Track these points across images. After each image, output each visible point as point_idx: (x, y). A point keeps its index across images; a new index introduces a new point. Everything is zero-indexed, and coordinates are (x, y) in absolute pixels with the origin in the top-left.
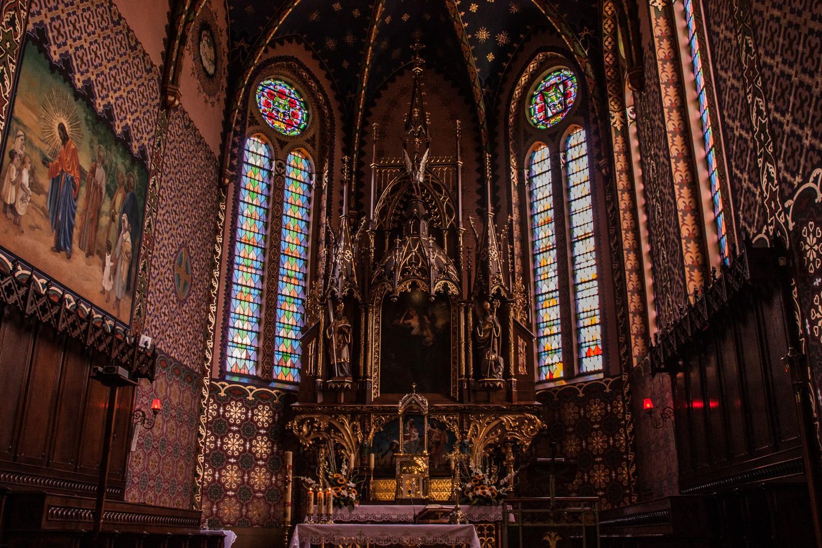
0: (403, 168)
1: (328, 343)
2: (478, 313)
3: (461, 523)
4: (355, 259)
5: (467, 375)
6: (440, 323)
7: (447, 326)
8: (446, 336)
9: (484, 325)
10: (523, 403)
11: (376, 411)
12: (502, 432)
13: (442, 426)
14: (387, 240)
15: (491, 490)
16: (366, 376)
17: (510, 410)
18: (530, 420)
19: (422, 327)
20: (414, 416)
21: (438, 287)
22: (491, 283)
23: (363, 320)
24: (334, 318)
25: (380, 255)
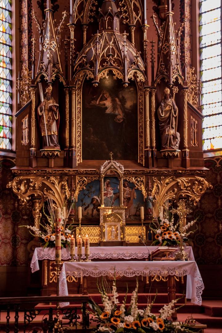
1: (39, 119)
2: (160, 98)
3: (186, 260)
4: (59, 48)
5: (151, 147)
6: (129, 104)
7: (135, 107)
8: (133, 115)
9: (165, 107)
10: (194, 168)
11: (80, 174)
12: (178, 191)
13: (132, 186)
14: (85, 33)
15: (176, 235)
16: (71, 146)
17: (184, 174)
18: (199, 182)
19: (114, 107)
20: (113, 178)
21: (129, 75)
22: (171, 73)
23: (67, 100)
24: (44, 98)
25: (80, 46)
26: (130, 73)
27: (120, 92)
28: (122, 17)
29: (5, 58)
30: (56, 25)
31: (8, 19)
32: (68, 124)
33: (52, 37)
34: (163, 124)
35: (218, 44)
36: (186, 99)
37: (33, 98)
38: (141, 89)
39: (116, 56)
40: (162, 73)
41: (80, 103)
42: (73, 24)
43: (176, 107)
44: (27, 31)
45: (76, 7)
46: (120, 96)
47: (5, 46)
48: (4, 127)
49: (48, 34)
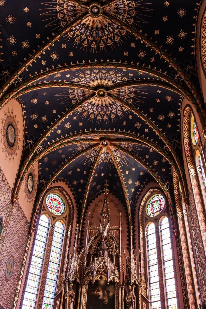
0: (99, 230)
1: (65, 301)
2: (127, 290)
4: (78, 265)
6: (111, 294)
7: (114, 295)
9: (129, 296)
14: (91, 258)
19: (104, 296)
21: (110, 279)
22: (132, 278)
24: (68, 290)
25: (88, 264)
26: (110, 278)
27: (107, 288)
28: (109, 251)
29: (55, 270)
30: (78, 254)
31: (59, 252)
32: (79, 304)
33: (75, 260)
34: (128, 305)
35: (156, 264)
36: (140, 291)
37: (63, 289)
38: (117, 286)
39: (104, 269)
40: (127, 278)
41: (86, 293)
42: (86, 254)
43: (135, 296)
44: (67, 258)
45: (88, 247)
46: (107, 290)
47: (56, 264)
48: (50, 305)
49: (74, 259)
